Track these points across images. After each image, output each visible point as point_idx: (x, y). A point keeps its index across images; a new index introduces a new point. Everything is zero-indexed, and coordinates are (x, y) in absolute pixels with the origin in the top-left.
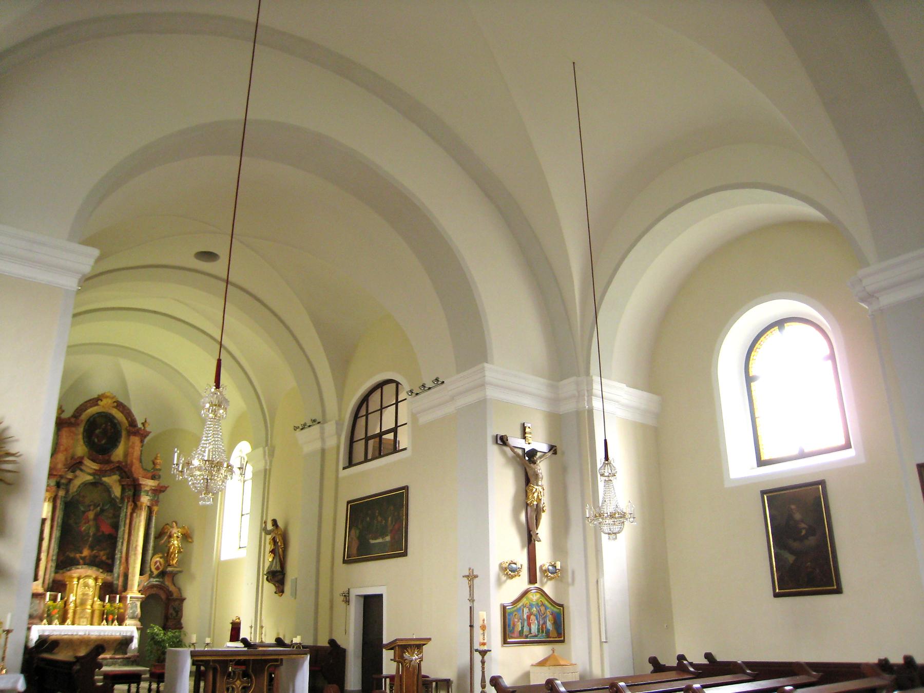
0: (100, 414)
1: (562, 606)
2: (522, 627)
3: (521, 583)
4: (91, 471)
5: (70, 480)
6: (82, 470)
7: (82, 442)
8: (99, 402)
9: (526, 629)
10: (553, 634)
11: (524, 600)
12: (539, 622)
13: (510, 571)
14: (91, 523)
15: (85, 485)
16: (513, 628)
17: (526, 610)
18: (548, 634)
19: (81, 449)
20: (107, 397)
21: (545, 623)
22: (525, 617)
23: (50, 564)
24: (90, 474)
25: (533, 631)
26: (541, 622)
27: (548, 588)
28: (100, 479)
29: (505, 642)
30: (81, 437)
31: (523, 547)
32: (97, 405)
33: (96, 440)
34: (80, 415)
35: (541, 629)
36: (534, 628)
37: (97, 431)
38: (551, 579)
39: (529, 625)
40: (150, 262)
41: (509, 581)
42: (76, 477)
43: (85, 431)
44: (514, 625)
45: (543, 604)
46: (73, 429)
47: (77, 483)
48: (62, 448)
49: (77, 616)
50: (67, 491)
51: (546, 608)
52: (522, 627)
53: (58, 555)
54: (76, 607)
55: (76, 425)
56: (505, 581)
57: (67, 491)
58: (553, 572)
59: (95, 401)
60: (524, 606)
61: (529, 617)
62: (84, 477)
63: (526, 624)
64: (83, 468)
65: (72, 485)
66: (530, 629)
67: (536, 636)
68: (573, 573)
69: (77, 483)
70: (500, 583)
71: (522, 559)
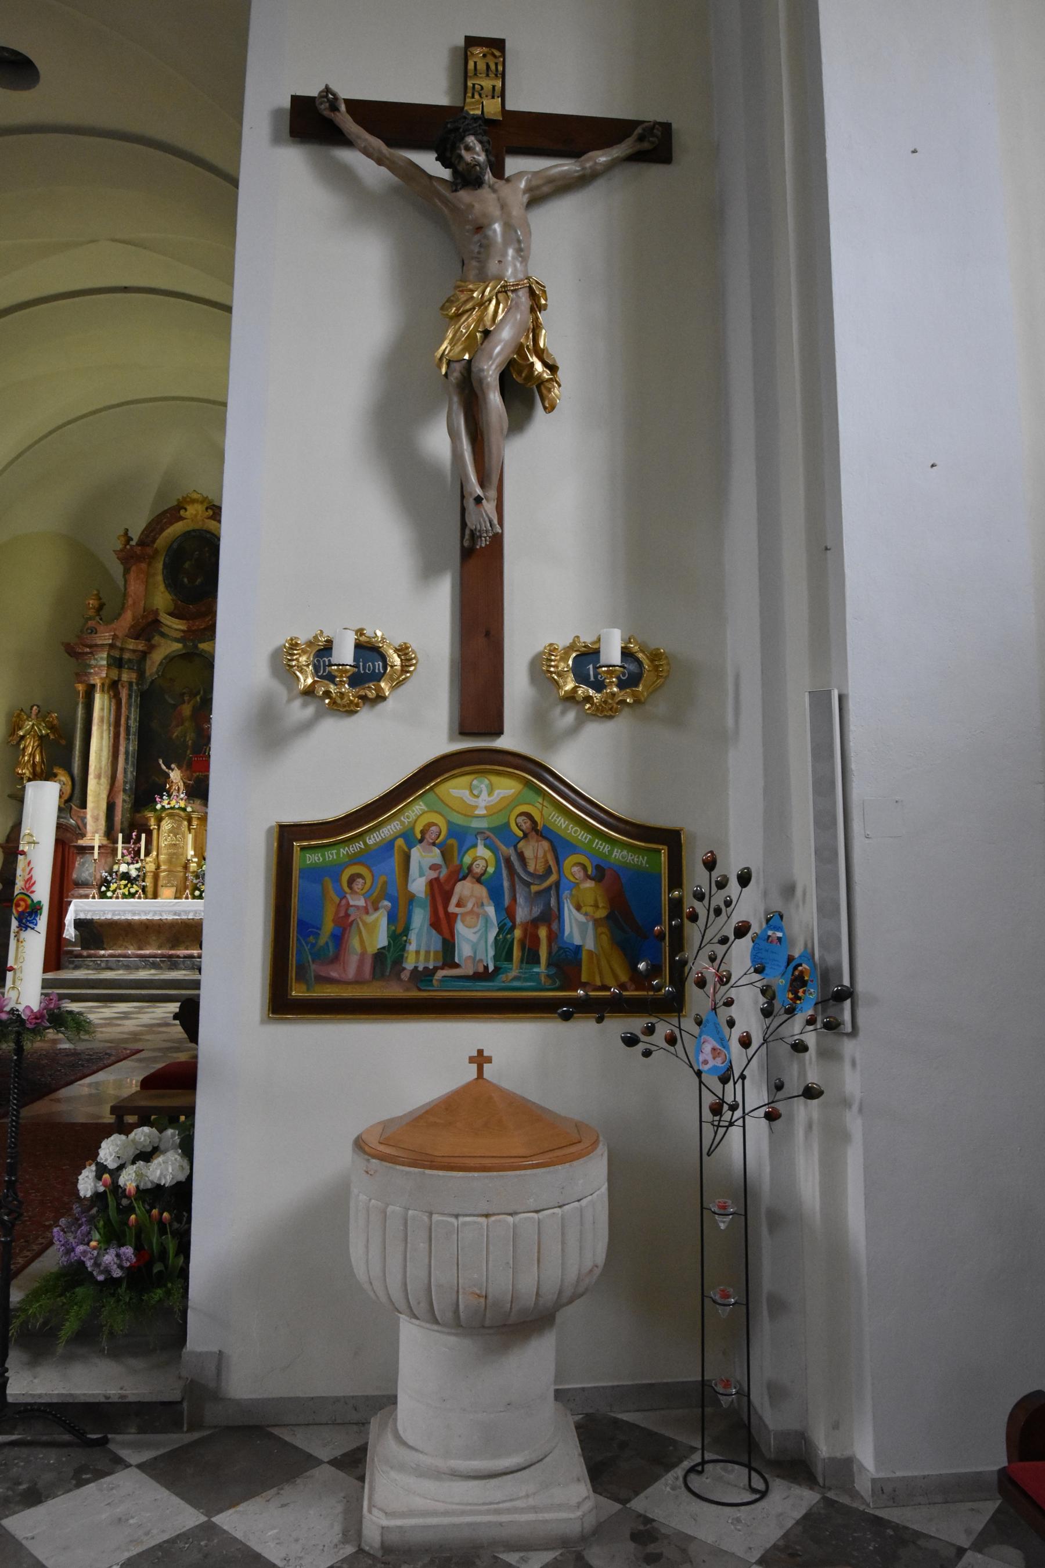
0: (187, 535)
1: (671, 839)
2: (398, 938)
3: (415, 725)
4: (179, 635)
5: (144, 655)
6: (163, 635)
7: (162, 587)
8: (182, 512)
9: (420, 947)
10: (606, 973)
11: (416, 812)
12: (507, 914)
13: (364, 675)
14: (187, 724)
15: (170, 659)
16: (339, 939)
17: (424, 860)
18: (567, 964)
19: (162, 599)
20: (193, 501)
21: (550, 917)
22: (418, 885)
23: (120, 799)
24: (177, 640)
25: (464, 950)
26: (522, 914)
27: (588, 760)
28: (196, 647)
29: (281, 1004)
30: (160, 578)
31: (428, 571)
32: (181, 518)
33: (186, 580)
34: (154, 541)
35: (515, 944)
36: (475, 940)
37: (187, 565)
38: (605, 712)
39: (443, 924)
40: (162, 136)
41: (333, 730)
42: (152, 648)
43: (164, 565)
44: (344, 926)
45: (536, 830)
46: (144, 566)
47: (157, 657)
48: (130, 601)
49: (160, 883)
50: (141, 674)
51: (559, 847)
52: (398, 938)
53: (137, 779)
54: (158, 867)
55: (151, 559)
56: (306, 727)
57: (141, 674)
58: (627, 684)
59: (174, 513)
60: (410, 839)
61: (441, 891)
62: (166, 648)
63: (420, 918)
64: (164, 630)
65: (148, 662)
66: (449, 947)
67: (483, 976)
68: (737, 677)
69: (157, 657)
70: (269, 733)
71: (424, 623)
